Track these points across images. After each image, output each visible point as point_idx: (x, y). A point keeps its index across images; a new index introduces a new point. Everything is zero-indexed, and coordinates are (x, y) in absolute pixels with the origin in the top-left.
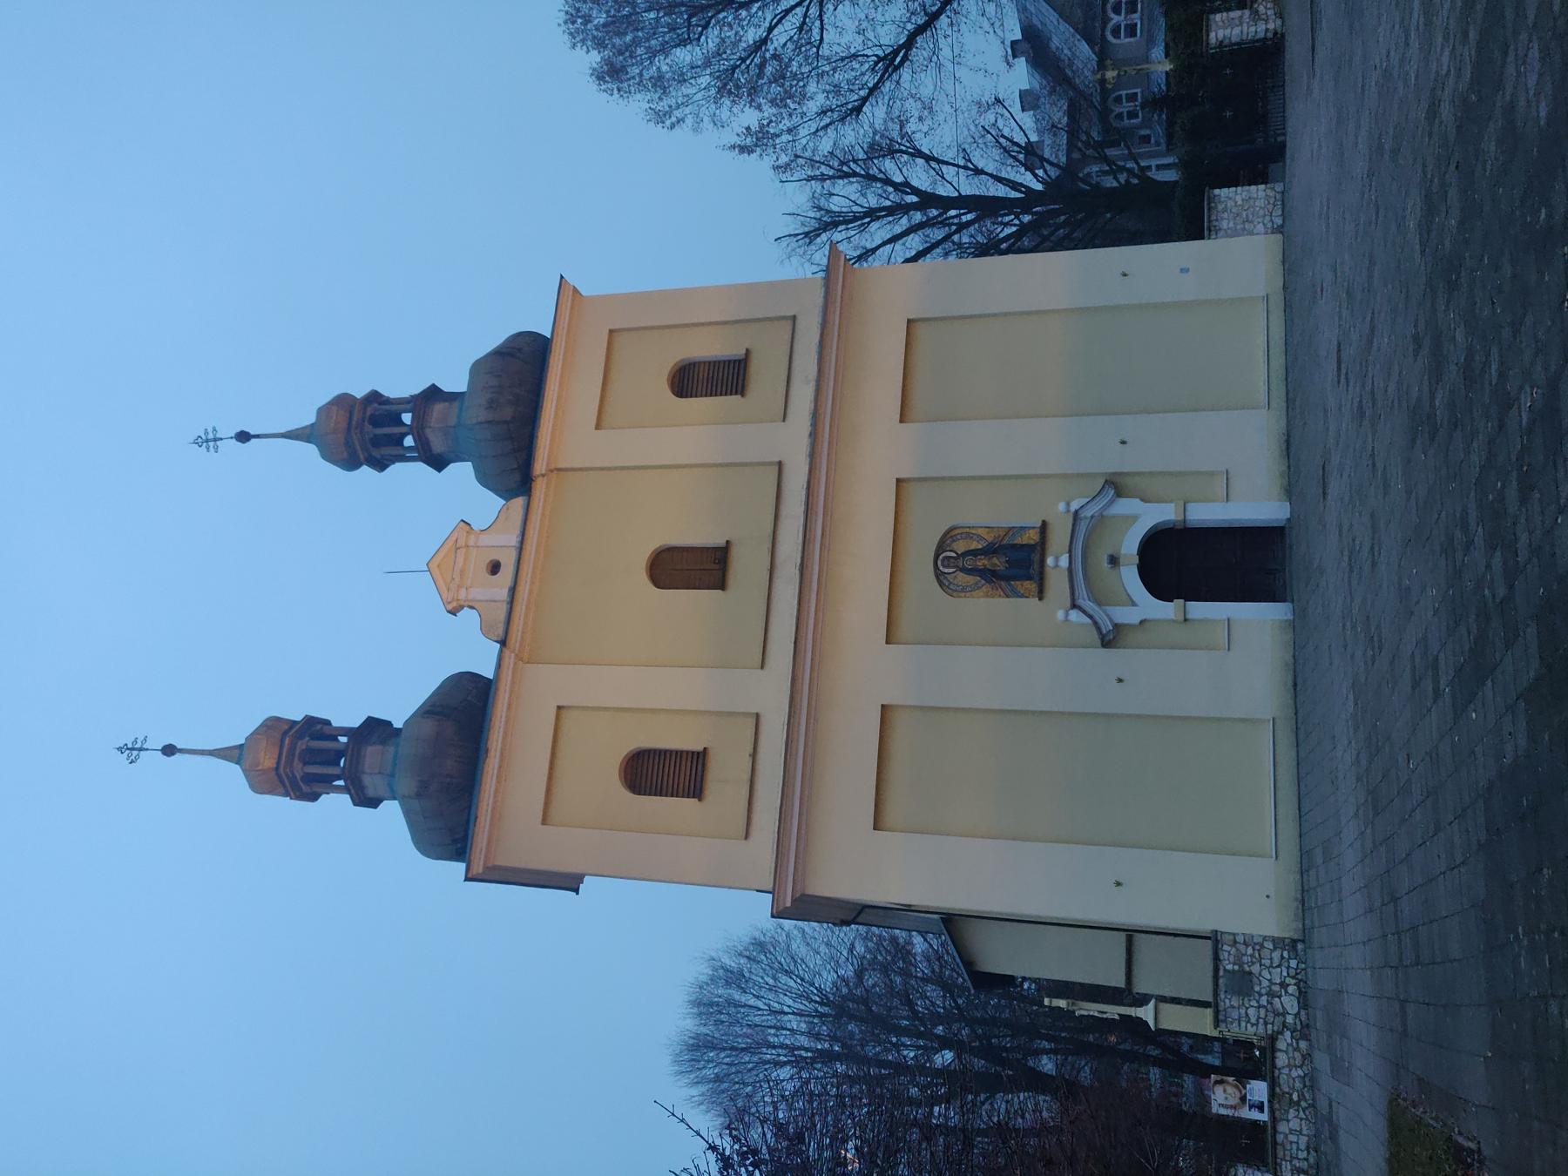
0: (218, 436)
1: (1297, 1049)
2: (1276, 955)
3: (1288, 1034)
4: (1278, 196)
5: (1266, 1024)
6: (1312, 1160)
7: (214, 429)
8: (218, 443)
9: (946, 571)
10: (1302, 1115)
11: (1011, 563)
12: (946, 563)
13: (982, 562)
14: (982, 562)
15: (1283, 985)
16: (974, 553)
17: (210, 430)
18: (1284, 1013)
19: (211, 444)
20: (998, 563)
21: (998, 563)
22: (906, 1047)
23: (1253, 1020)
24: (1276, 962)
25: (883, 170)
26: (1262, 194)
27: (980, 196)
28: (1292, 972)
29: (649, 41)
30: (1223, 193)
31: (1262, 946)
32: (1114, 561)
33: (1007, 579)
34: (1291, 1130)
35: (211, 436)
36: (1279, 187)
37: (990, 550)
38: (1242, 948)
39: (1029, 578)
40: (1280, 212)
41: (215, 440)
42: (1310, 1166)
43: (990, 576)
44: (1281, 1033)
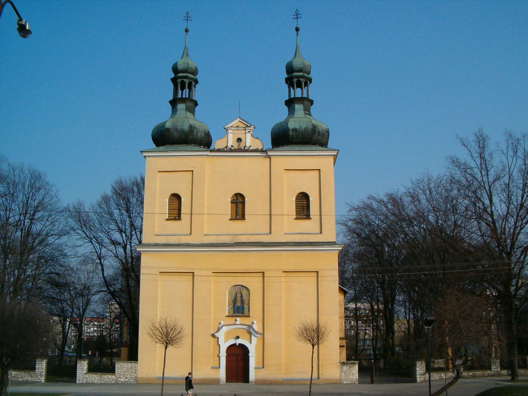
0: (188, 21)
1: (112, 380)
2: (133, 377)
3: (116, 378)
4: (353, 383)
5: (118, 373)
6: (89, 382)
7: (301, 18)
8: (296, 19)
9: (236, 288)
10: (99, 380)
11: (238, 307)
12: (239, 288)
13: (239, 298)
14: (239, 298)
15: (127, 378)
16: (242, 297)
17: (294, 17)
18: (120, 378)
19: (299, 16)
20: (239, 304)
21: (239, 304)
22: (45, 270)
23: (118, 370)
24: (132, 376)
25: (445, 256)
26: (354, 377)
27: (76, 368)
28: (130, 380)
29: (37, 264)
30: (356, 367)
31: (135, 373)
32: (238, 337)
33: (234, 306)
34: (95, 378)
35: (189, 19)
36: (357, 383)
37: (242, 302)
38: (135, 369)
39: (234, 313)
40: (347, 383)
41: (187, 20)
42: (88, 381)
43: (235, 301)
44: (116, 377)
